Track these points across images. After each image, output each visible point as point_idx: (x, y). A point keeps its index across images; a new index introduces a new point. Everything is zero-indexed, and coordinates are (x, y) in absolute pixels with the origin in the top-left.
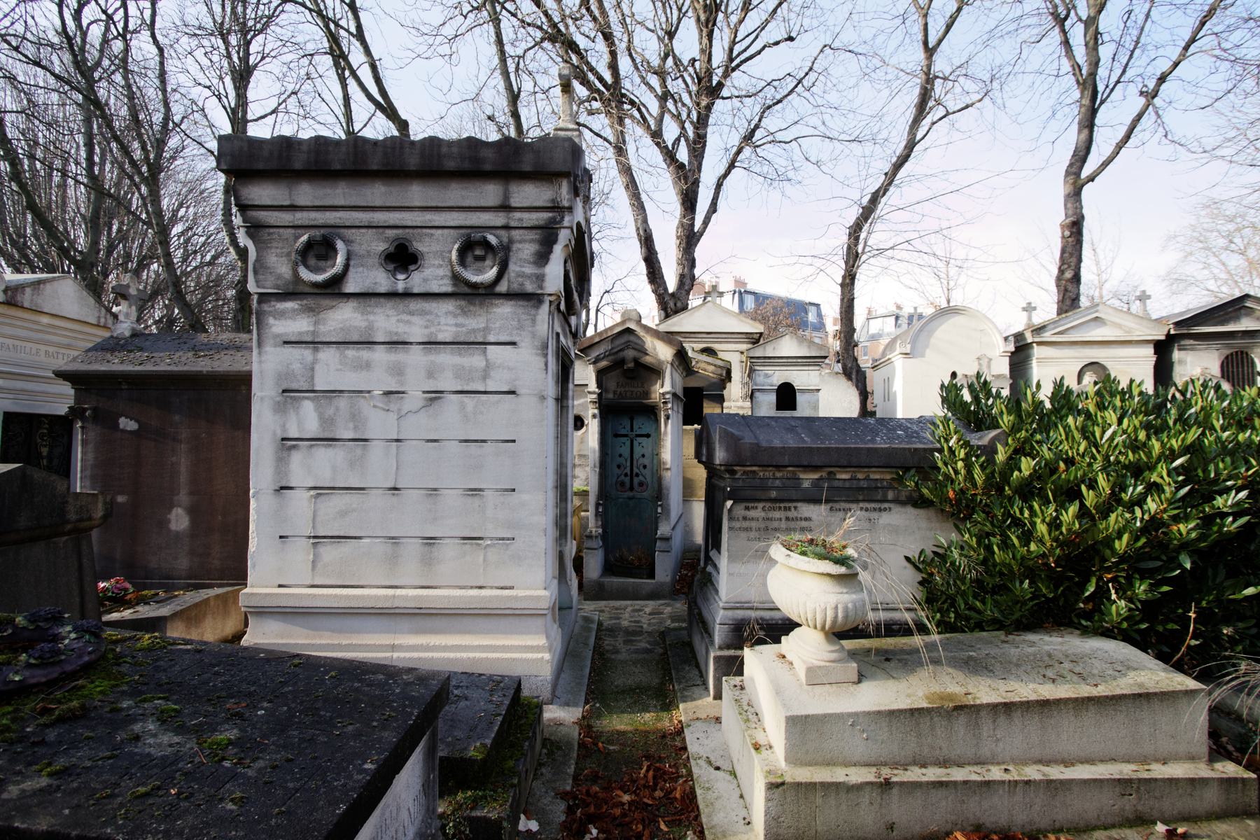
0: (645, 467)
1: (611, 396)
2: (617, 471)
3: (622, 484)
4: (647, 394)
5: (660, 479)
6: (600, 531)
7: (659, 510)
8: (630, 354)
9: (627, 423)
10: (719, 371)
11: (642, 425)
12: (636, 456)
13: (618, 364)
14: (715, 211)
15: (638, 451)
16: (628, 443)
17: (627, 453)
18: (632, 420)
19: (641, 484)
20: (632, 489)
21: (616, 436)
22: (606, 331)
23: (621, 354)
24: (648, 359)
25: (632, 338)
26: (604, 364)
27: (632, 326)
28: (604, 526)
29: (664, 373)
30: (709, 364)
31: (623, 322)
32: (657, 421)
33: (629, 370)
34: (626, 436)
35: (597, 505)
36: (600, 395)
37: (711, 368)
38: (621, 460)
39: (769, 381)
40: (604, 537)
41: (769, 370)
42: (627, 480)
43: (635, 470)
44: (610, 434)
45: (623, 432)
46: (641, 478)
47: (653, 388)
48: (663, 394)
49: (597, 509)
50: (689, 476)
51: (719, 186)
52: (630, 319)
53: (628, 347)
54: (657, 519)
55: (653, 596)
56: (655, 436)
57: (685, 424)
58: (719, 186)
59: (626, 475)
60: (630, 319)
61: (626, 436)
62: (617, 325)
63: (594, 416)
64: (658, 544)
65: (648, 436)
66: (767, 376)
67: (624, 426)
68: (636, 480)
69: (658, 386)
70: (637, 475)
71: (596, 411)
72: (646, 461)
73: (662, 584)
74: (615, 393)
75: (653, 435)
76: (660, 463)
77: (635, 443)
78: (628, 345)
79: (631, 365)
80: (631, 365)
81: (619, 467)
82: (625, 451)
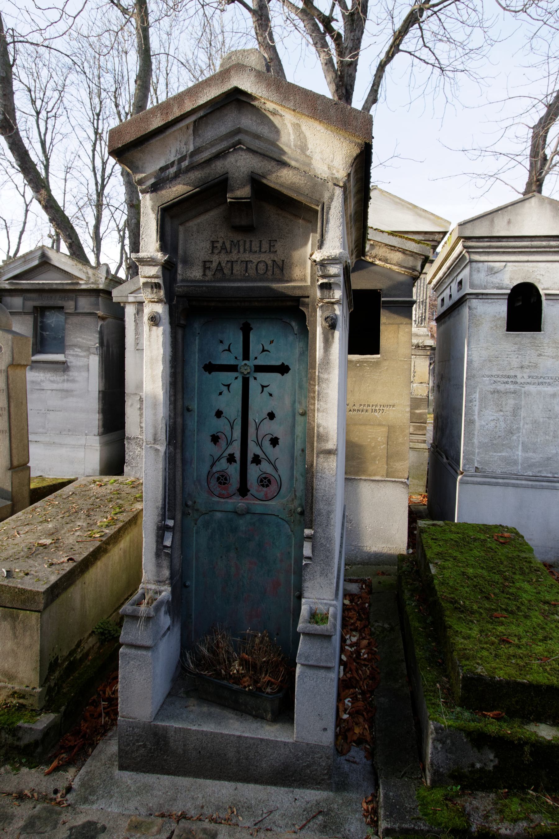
0: (274, 442)
1: (196, 273)
2: (209, 448)
3: (223, 479)
4: (282, 269)
5: (309, 475)
6: (166, 592)
7: (307, 550)
8: (240, 164)
9: (235, 338)
10: (410, 261)
11: (270, 343)
12: (253, 416)
13: (212, 193)
14: (375, 101)
15: (259, 404)
16: (237, 386)
17: (233, 409)
18: (246, 331)
19: (265, 481)
20: (243, 491)
21: (210, 368)
22: (180, 98)
23: (219, 166)
24: (284, 179)
25: (247, 121)
26: (177, 190)
27: (246, 84)
28: (179, 582)
29: (325, 209)
30: (393, 248)
31: (224, 74)
32: (305, 333)
33: (239, 206)
34: (233, 368)
35: (161, 530)
36: (168, 268)
37: (397, 257)
38: (221, 425)
39: (495, 279)
40: (177, 606)
41: (496, 261)
42: (234, 470)
43: (253, 449)
44: (195, 363)
45: (226, 359)
46: (265, 466)
47: (297, 255)
48: (323, 264)
49: (160, 538)
50: (355, 439)
51: (381, 68)
52: (240, 67)
53: (235, 147)
54: (300, 571)
55: (288, 775)
56: (296, 370)
57: (351, 352)
58: (381, 68)
59: (231, 459)
60: (240, 67)
61: (233, 368)
62: (208, 82)
63: (154, 320)
64: (303, 645)
65: (283, 369)
66: (492, 272)
67: (227, 343)
68: (254, 472)
69: (309, 248)
70: (257, 460)
71: (159, 309)
72: (276, 428)
73: (312, 749)
74: (206, 265)
75: (295, 367)
76: (311, 435)
77: (254, 386)
78: (235, 142)
79: (244, 192)
80: (244, 192)
81: (215, 439)
82: (231, 404)
